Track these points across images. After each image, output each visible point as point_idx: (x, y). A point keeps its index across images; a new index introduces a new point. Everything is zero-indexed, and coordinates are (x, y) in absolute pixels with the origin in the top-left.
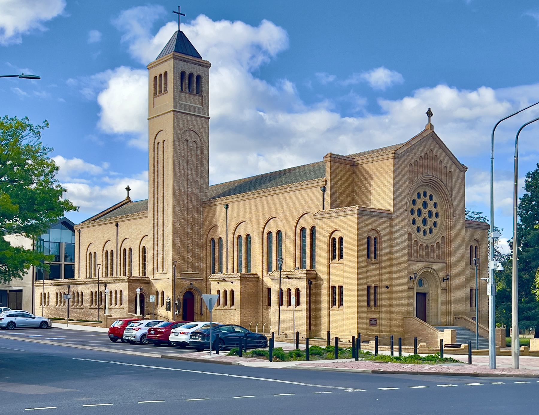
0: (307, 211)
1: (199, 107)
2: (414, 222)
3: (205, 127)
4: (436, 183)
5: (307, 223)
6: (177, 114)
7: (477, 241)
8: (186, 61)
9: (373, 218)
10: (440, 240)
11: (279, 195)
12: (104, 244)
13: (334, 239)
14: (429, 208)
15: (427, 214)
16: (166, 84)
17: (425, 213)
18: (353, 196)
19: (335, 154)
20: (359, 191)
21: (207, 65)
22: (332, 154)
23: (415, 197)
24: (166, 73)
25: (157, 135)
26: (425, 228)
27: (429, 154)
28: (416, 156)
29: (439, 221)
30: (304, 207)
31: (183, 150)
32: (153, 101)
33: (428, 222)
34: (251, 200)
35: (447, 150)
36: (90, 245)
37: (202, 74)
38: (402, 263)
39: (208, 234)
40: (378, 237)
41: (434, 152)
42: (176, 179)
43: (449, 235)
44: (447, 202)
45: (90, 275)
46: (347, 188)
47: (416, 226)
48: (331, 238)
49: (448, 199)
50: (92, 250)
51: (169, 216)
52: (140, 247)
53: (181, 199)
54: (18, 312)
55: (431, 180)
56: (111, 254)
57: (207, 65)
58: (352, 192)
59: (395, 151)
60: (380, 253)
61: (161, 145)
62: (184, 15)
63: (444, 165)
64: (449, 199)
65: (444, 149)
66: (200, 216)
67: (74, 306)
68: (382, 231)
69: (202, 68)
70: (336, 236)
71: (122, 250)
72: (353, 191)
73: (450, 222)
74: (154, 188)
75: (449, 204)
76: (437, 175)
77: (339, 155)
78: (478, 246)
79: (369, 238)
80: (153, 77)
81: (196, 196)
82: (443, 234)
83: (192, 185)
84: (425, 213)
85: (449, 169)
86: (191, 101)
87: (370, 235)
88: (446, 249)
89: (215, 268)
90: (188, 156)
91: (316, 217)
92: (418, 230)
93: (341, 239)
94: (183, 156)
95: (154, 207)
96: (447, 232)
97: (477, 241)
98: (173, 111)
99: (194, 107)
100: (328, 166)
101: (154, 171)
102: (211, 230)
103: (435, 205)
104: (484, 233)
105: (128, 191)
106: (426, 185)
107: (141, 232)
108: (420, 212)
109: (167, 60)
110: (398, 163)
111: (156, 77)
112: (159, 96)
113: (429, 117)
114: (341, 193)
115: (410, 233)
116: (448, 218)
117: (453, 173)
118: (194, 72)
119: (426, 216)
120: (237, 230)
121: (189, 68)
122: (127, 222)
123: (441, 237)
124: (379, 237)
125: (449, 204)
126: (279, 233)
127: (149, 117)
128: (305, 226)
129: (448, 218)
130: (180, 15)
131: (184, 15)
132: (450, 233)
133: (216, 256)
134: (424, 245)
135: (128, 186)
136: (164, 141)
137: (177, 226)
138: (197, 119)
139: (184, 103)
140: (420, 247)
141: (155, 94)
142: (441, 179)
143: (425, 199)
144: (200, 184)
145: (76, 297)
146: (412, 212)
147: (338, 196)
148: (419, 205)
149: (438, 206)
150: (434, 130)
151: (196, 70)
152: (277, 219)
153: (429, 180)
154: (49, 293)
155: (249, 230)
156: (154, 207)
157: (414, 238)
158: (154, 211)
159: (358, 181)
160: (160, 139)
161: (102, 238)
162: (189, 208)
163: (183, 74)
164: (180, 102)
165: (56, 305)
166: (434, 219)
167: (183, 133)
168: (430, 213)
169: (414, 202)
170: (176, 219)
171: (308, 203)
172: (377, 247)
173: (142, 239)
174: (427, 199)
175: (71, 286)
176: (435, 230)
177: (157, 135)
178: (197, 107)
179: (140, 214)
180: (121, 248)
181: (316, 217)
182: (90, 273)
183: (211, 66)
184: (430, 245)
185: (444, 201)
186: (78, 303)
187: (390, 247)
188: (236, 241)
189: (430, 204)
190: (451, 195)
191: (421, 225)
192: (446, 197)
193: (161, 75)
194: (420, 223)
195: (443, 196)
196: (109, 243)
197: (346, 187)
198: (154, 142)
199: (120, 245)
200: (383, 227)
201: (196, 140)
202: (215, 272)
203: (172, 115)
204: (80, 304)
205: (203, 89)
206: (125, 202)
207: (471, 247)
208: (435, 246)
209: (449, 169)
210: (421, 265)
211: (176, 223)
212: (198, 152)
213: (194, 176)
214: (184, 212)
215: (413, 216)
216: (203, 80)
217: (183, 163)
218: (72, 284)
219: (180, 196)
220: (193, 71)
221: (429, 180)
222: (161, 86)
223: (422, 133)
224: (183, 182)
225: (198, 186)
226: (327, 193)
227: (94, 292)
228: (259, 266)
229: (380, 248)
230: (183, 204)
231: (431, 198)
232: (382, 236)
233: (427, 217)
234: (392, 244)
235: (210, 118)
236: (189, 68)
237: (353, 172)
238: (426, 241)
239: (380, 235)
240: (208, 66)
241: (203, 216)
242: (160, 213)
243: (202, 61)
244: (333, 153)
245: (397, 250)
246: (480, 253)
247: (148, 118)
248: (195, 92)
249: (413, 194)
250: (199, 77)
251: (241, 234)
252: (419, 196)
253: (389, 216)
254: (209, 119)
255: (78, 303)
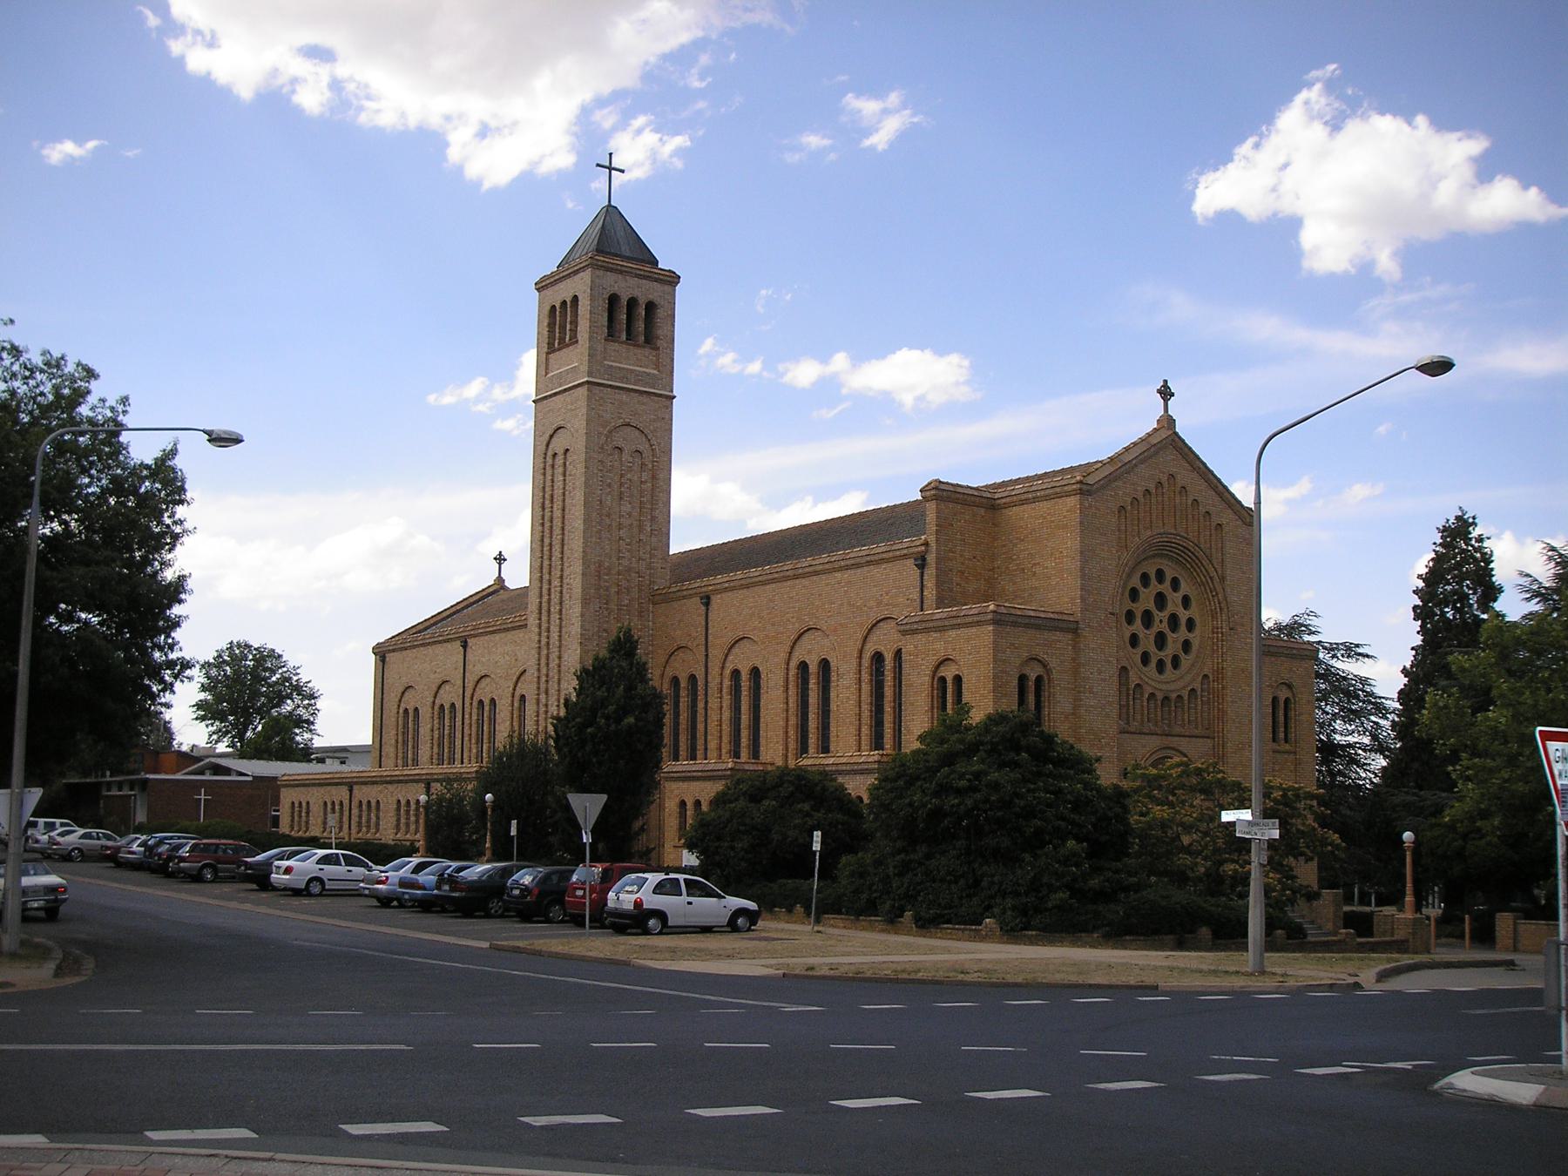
0: (886, 613)
1: (648, 374)
2: (1134, 641)
3: (663, 418)
4: (1187, 552)
5: (885, 640)
6: (596, 390)
7: (1289, 686)
8: (621, 272)
9: (1031, 632)
10: (1197, 685)
11: (824, 577)
12: (436, 689)
13: (943, 680)
14: (1170, 608)
15: (1165, 623)
16: (575, 323)
17: (1161, 621)
18: (994, 579)
19: (947, 483)
20: (1007, 568)
21: (672, 279)
22: (940, 482)
23: (1135, 581)
24: (575, 299)
25: (551, 436)
26: (1161, 654)
27: (1166, 485)
28: (1136, 490)
29: (1195, 638)
30: (879, 603)
31: (609, 471)
32: (547, 359)
33: (1170, 640)
34: (762, 587)
35: (1210, 475)
36: (405, 690)
37: (657, 300)
38: (1103, 738)
39: (665, 667)
40: (1046, 677)
41: (1179, 477)
42: (591, 537)
43: (1219, 673)
44: (1213, 596)
45: (403, 763)
46: (978, 561)
47: (1139, 651)
48: (936, 678)
49: (1215, 589)
50: (410, 702)
51: (573, 624)
52: (860, 657)
53: (602, 584)
54: (757, 761)
55: (1173, 545)
56: (451, 712)
57: (672, 279)
58: (990, 570)
59: (1084, 476)
60: (1049, 714)
61: (559, 461)
62: (598, 165)
63: (1202, 510)
64: (1219, 589)
65: (1203, 473)
66: (646, 623)
67: (360, 835)
68: (1053, 663)
69: (659, 285)
70: (949, 673)
71: (475, 704)
72: (993, 569)
73: (1222, 641)
74: (542, 557)
75: (1219, 600)
76: (1176, 529)
77: (958, 485)
78: (1291, 698)
79: (1023, 679)
80: (548, 308)
81: (639, 577)
82: (1206, 671)
83: (628, 551)
84: (1161, 621)
85: (1215, 520)
86: (629, 360)
87: (1024, 672)
88: (1214, 705)
89: (681, 749)
90: (621, 485)
91: (903, 628)
92: (1145, 658)
93: (958, 680)
94: (609, 485)
95: (541, 603)
96: (1216, 666)
97: (1289, 686)
98: (588, 382)
99: (638, 374)
100: (931, 507)
101: (543, 518)
102: (673, 658)
103: (1186, 601)
104: (1306, 668)
105: (500, 564)
106: (1161, 556)
107: (516, 660)
108: (1148, 619)
109: (577, 270)
110: (1090, 506)
111: (553, 307)
112: (559, 349)
113: (1166, 401)
114: (962, 573)
115: (1123, 667)
116: (1217, 633)
117: (1226, 529)
118: (639, 294)
119: (1165, 627)
120: (730, 658)
121: (626, 287)
122: (486, 638)
123: (1200, 678)
124: (1048, 675)
125: (1219, 600)
126: (825, 665)
127: (536, 396)
128: (882, 649)
129: (1217, 633)
130: (608, 164)
131: (598, 165)
132: (1223, 668)
133: (813, 699)
134: (1160, 696)
135: (500, 552)
136: (567, 450)
137: (590, 647)
138: (644, 399)
139: (614, 364)
140: (1148, 700)
141: (550, 344)
142: (1196, 542)
143: (1160, 588)
144: (648, 548)
145: (365, 814)
146: (1130, 616)
147: (956, 579)
148: (1147, 601)
149: (1194, 603)
150: (1177, 430)
151: (643, 291)
152: (820, 633)
153: (1169, 544)
154: (308, 803)
155: (757, 656)
156: (541, 603)
157: (1134, 679)
158: (540, 613)
159: (1004, 546)
160: (558, 444)
161: (432, 676)
162: (621, 605)
163: (613, 300)
164: (606, 362)
165: (323, 832)
166: (1183, 632)
167: (610, 432)
168: (1174, 621)
169: (1134, 594)
170: (589, 630)
171: (887, 594)
172: (1042, 699)
173: (519, 678)
174: (1166, 587)
175: (355, 787)
176: (1186, 661)
177: (551, 436)
178: (645, 373)
179: (517, 619)
180: (472, 699)
181: (903, 628)
182: (405, 754)
183: (679, 282)
184: (1174, 696)
185: (1207, 593)
186: (368, 827)
187: (1075, 700)
188: (727, 683)
189: (1174, 599)
190: (1223, 579)
191: (1152, 649)
192: (1211, 584)
193: (564, 303)
194: (1147, 641)
195: (1204, 580)
196: (447, 687)
197: (974, 558)
198: (545, 454)
199: (470, 693)
200: (1056, 650)
201: (641, 448)
202: (681, 758)
203: (586, 393)
204: (373, 831)
205: (659, 332)
206: (491, 590)
207: (1275, 700)
208: (1186, 698)
209: (1215, 520)
210: (1154, 742)
211: (589, 639)
212: (645, 476)
213: (635, 530)
214: (609, 614)
215: (1131, 628)
216: (661, 313)
217: (608, 500)
218: (356, 783)
219: (599, 577)
220: (636, 293)
221: (1169, 544)
222: (563, 327)
223: (1149, 435)
224: (608, 544)
225: (644, 553)
226: (930, 572)
227: (403, 802)
228: (777, 742)
229: (1049, 703)
230: (608, 596)
231: (1175, 584)
232: (1055, 675)
233: (1167, 631)
234: (1079, 692)
235: (674, 397)
236: (629, 287)
237: (993, 524)
238: (1164, 687)
239: (1048, 672)
240: (673, 282)
241: (654, 623)
242: (555, 617)
243: (659, 272)
244: (942, 480)
245: (1092, 706)
246: (1295, 714)
247: (534, 398)
248: (624, 337)
249: (1129, 576)
250: (651, 307)
251: (740, 667)
252: (1145, 579)
253: (1073, 626)
254: (674, 400)
255: (368, 827)
